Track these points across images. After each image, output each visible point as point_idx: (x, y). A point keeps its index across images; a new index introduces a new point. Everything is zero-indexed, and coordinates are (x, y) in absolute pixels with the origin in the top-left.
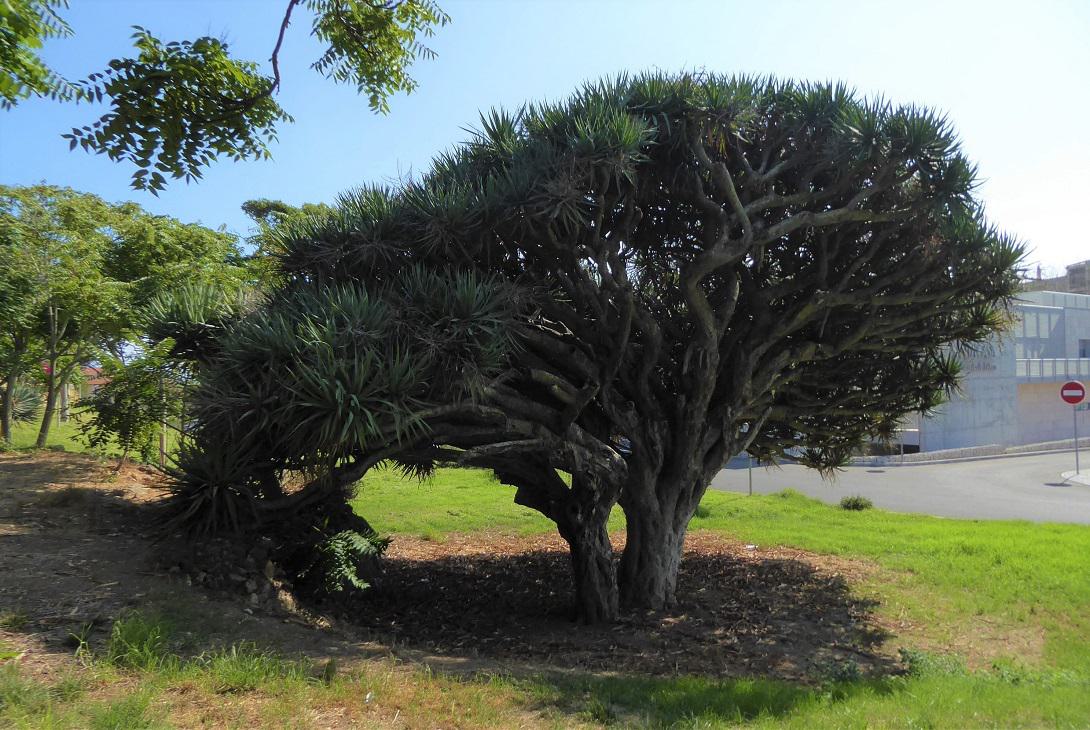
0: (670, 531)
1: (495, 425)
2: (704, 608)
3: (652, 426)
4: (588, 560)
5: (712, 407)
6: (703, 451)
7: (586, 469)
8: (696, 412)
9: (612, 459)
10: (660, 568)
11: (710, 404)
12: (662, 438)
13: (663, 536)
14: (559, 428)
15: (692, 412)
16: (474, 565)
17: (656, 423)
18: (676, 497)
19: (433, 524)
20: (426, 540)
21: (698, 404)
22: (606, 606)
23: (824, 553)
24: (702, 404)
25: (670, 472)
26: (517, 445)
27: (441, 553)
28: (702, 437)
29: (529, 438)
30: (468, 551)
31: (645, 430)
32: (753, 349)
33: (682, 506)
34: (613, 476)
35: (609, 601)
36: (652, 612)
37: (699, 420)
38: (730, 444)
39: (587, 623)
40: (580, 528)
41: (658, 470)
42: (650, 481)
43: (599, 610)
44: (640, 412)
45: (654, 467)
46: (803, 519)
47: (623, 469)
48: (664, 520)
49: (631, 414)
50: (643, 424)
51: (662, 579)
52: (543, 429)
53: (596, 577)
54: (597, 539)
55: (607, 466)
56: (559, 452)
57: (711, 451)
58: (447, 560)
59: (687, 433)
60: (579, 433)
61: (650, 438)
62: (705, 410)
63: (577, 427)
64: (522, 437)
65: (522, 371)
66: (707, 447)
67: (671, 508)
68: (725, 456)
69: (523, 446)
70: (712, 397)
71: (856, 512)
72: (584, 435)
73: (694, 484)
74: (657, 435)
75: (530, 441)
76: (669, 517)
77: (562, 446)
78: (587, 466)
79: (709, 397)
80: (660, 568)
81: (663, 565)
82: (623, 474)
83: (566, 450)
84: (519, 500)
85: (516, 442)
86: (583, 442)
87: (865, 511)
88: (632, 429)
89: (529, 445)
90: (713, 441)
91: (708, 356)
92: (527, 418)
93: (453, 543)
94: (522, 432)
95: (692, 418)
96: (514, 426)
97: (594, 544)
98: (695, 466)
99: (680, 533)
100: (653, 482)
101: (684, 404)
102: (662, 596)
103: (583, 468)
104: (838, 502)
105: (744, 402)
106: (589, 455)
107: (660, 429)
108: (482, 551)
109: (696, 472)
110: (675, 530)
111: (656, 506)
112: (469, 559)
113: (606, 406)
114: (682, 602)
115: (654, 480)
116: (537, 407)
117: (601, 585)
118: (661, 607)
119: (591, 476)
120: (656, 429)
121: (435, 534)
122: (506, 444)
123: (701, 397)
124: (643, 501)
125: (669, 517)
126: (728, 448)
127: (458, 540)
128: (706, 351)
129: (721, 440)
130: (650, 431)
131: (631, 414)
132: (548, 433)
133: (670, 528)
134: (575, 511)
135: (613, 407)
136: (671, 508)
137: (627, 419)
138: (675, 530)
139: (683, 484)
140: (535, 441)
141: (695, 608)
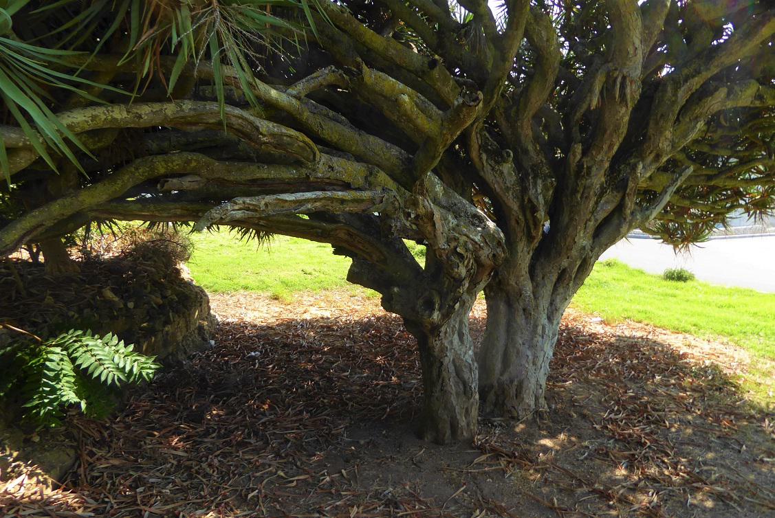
0: (544, 320)
1: (298, 164)
2: (584, 417)
3: (535, 184)
4: (442, 363)
5: (616, 161)
6: (596, 220)
7: (453, 244)
8: (594, 169)
9: (485, 228)
10: (530, 367)
11: (614, 157)
12: (546, 202)
13: (536, 326)
14: (408, 178)
15: (589, 168)
16: (316, 333)
17: (539, 182)
18: (554, 279)
19: (285, 284)
20: (276, 299)
21: (599, 157)
22: (463, 422)
23: (677, 331)
24: (603, 158)
25: (548, 248)
26: (331, 199)
27: (287, 316)
28: (597, 203)
29: (359, 189)
30: (313, 313)
31: (524, 190)
32: (686, 81)
33: (561, 290)
34: (485, 253)
35: (467, 412)
36: (522, 426)
37: (598, 179)
38: (632, 213)
39: (438, 442)
40: (435, 329)
41: (536, 244)
42: (524, 257)
43: (454, 426)
44: (519, 166)
45: (530, 238)
46: (634, 288)
47: (499, 243)
48: (537, 306)
49: (507, 167)
50: (522, 181)
51: (533, 381)
52: (382, 177)
53: (452, 385)
54: (456, 336)
55: (478, 238)
56: (409, 215)
57: (607, 221)
58: (289, 325)
59: (579, 196)
60: (439, 189)
61: (530, 200)
62: (607, 165)
63: (436, 180)
64: (347, 186)
65: (348, 72)
66: (601, 216)
67: (546, 291)
68: (624, 229)
69: (343, 201)
70: (621, 145)
71: (681, 284)
72: (446, 193)
73: (578, 263)
74: (541, 198)
75: (358, 194)
76: (544, 303)
77: (415, 204)
78: (456, 239)
79: (616, 148)
80: (530, 367)
81: (534, 364)
82: (499, 250)
83: (421, 211)
84: (353, 277)
85: (329, 194)
86: (444, 203)
87: (689, 282)
88: (508, 189)
89: (355, 201)
90: (610, 208)
91: (628, 83)
92: (359, 158)
93: (300, 303)
94: (345, 178)
95: (589, 173)
96: (332, 168)
97: (451, 342)
98: (583, 239)
99: (555, 322)
100: (528, 258)
101: (579, 157)
102: (532, 402)
103: (448, 242)
104: (662, 273)
105: (658, 157)
106: (453, 222)
107: (546, 188)
108: (327, 314)
109: (584, 248)
110: (550, 319)
111: (528, 287)
112: (309, 325)
113: (474, 154)
114: (553, 406)
115: (529, 257)
116: (375, 144)
117: (458, 394)
118: (530, 417)
119: (461, 256)
120: (539, 191)
121: (284, 293)
122: (308, 195)
123: (605, 147)
124: (512, 282)
125: (544, 303)
126: (629, 218)
127: (307, 299)
128: (624, 78)
129: (620, 208)
130: (532, 192)
131: (507, 167)
132: (391, 184)
133: (545, 316)
134: (430, 306)
135: (484, 156)
136: (546, 291)
137: (502, 173)
138: (550, 319)
139: (565, 263)
140: (366, 194)
141: (571, 416)
